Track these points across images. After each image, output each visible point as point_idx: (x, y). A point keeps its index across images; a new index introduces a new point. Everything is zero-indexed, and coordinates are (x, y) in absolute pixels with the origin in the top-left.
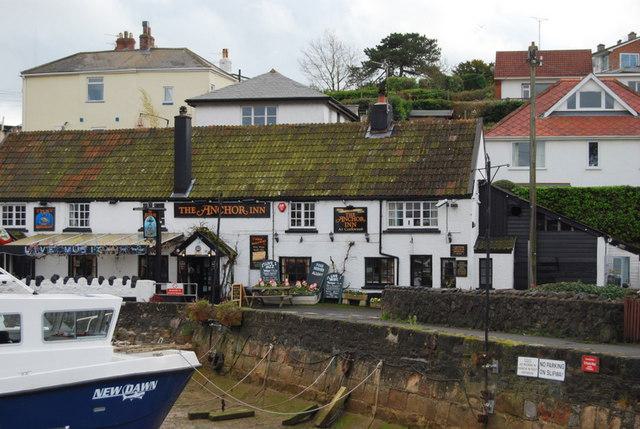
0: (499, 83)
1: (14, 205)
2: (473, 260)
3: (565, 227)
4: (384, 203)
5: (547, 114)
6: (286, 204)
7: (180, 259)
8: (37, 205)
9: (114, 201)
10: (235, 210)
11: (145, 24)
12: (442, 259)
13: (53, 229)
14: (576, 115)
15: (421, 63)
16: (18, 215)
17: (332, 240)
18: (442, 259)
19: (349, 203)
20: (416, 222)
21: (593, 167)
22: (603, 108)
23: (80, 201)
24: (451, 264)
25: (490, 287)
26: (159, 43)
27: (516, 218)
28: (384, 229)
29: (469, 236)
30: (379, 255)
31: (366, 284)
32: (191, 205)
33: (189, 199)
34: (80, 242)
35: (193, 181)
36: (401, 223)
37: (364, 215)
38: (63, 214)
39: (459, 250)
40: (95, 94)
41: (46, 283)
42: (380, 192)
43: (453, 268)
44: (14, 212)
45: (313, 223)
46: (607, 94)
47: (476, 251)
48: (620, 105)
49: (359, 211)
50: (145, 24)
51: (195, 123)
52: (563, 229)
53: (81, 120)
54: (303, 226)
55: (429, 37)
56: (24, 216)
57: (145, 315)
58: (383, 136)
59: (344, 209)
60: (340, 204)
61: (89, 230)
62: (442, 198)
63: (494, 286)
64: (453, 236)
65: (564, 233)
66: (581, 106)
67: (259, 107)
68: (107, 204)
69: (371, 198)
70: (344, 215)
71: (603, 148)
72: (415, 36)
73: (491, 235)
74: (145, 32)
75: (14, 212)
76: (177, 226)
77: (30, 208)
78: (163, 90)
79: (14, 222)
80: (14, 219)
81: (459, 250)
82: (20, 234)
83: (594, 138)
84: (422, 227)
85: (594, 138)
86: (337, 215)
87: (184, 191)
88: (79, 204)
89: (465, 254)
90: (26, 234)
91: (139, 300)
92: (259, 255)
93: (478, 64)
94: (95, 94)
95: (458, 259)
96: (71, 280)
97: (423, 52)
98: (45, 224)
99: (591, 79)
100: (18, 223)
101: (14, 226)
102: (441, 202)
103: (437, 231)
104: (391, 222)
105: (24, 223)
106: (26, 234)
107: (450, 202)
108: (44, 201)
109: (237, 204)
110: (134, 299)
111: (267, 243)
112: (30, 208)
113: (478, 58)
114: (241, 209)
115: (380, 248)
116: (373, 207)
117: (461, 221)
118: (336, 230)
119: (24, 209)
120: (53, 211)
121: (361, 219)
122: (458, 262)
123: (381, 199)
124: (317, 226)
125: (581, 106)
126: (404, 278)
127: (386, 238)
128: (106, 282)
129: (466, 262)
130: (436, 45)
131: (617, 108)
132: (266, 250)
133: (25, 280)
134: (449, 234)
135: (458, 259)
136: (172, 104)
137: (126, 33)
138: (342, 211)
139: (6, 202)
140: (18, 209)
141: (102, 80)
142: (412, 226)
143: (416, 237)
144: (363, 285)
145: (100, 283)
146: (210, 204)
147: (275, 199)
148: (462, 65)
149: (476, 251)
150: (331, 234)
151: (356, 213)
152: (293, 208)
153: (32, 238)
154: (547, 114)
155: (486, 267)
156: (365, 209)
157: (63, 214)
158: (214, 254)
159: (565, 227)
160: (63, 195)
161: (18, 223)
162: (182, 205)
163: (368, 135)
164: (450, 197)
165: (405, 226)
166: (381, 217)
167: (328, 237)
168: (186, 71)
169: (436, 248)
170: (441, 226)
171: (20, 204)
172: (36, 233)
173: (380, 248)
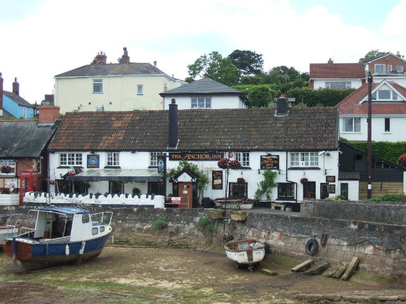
0: (312, 81)
1: (75, 153)
2: (338, 184)
3: (386, 166)
4: (289, 153)
5: (361, 102)
6: (233, 153)
7: (174, 184)
8: (89, 153)
9: (134, 151)
10: (204, 156)
11: (125, 49)
12: (321, 184)
13: (98, 167)
14: (376, 103)
15: (251, 68)
16: (77, 159)
17: (259, 173)
18: (321, 184)
19: (269, 153)
20: (307, 164)
21: (387, 132)
22: (391, 99)
23: (113, 150)
24: (326, 187)
25: (347, 198)
26: (132, 60)
27: (359, 161)
28: (289, 167)
29: (334, 171)
30: (286, 182)
31: (278, 197)
32: (179, 154)
33: (178, 150)
34: (113, 173)
35: (179, 140)
36: (298, 164)
37: (277, 159)
38: (103, 158)
39: (330, 179)
40: (97, 88)
41: (89, 196)
42: (287, 147)
43: (326, 189)
44: (75, 157)
45: (248, 164)
46: (393, 92)
47: (339, 179)
48: (400, 98)
49: (274, 157)
50: (125, 49)
51: (179, 108)
52: (384, 167)
53: (90, 103)
54: (113, 166)
55: (257, 52)
56: (81, 159)
57: (178, 215)
58: (284, 116)
59: (266, 156)
60: (264, 154)
61: (119, 168)
62: (321, 150)
63: (349, 199)
64: (328, 171)
65: (385, 169)
66: (379, 98)
67: (201, 98)
68: (130, 153)
69: (281, 151)
70: (266, 159)
71: (392, 122)
72: (249, 52)
73: (346, 169)
74: (125, 53)
75: (75, 157)
76: (172, 165)
77: (85, 155)
78: (136, 88)
79: (75, 163)
80: (75, 161)
81: (330, 179)
82: (78, 170)
83: (388, 116)
84: (310, 166)
85: (388, 116)
86: (262, 159)
87: (174, 146)
88: (113, 153)
89: (334, 181)
90: (82, 169)
91: (156, 207)
92: (217, 182)
93: (292, 72)
94: (97, 88)
95: (330, 183)
96: (110, 196)
97: (254, 61)
98: (93, 165)
99: (385, 84)
100: (77, 163)
101: (75, 165)
102: (320, 153)
103: (318, 169)
104: (292, 164)
105: (81, 163)
106: (82, 169)
107: (326, 153)
108: (93, 151)
109: (205, 154)
110: (153, 206)
111: (222, 174)
112: (85, 155)
113: (284, 65)
114: (207, 156)
115: (287, 178)
116: (282, 156)
117: (330, 163)
118: (262, 168)
119: (81, 155)
120: (98, 157)
121: (276, 162)
122: (330, 185)
123: (287, 151)
124: (251, 165)
125: (379, 98)
126: (299, 195)
127: (291, 173)
128: (94, 196)
129: (334, 185)
130: (261, 58)
131: (399, 99)
132: (222, 178)
133: (68, 195)
134: (326, 170)
135: (330, 183)
136: (142, 95)
137: (101, 53)
138: (265, 157)
139: (78, 151)
140: (77, 155)
141: (101, 81)
142: (304, 166)
143: (307, 172)
144: (277, 198)
145: (91, 197)
146: (190, 154)
147: (226, 150)
148: (275, 69)
149: (339, 179)
150: (259, 170)
151: (273, 158)
152: (237, 156)
153: (85, 172)
154: (361, 102)
155: (344, 187)
156: (278, 156)
157: (103, 158)
158: (194, 181)
159: (386, 166)
160: (104, 148)
161: (77, 163)
162: (173, 154)
163: (275, 115)
164: (326, 150)
165: (300, 166)
166: (287, 161)
167: (258, 172)
168: (150, 76)
169: (318, 178)
170: (320, 165)
171: (79, 153)
172: (88, 169)
173: (287, 178)
